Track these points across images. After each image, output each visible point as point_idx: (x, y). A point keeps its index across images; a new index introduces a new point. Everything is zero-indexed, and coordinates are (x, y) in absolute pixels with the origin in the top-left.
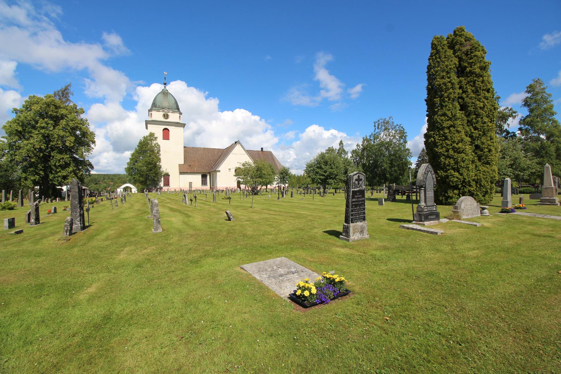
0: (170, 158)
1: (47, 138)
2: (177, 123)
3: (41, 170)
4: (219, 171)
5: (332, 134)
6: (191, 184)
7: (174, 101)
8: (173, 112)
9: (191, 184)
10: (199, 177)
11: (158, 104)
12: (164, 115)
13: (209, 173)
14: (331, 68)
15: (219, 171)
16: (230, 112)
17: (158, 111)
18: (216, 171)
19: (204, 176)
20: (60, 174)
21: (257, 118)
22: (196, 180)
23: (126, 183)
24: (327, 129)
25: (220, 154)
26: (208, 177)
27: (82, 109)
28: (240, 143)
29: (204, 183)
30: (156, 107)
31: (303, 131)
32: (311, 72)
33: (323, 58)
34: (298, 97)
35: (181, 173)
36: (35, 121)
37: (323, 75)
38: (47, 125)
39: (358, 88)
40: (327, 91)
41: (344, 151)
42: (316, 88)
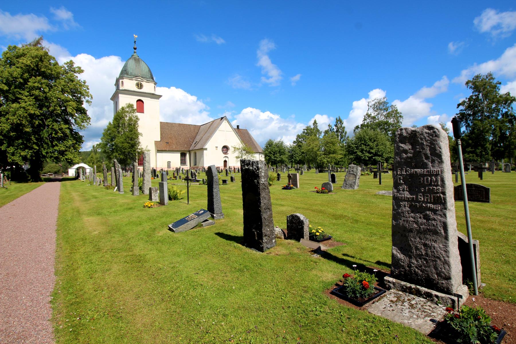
0: (148, 136)
1: (42, 102)
2: (153, 94)
3: (34, 143)
4: (206, 149)
5: (268, 116)
6: (169, 163)
7: (147, 70)
8: (148, 81)
9: (169, 163)
10: (178, 155)
11: (130, 70)
12: (137, 85)
13: (189, 151)
14: (273, 56)
15: (206, 149)
16: (167, 89)
17: (131, 79)
18: (202, 149)
19: (183, 155)
20: (56, 148)
21: (194, 98)
22: (175, 159)
23: (85, 163)
24: (263, 111)
25: (196, 131)
26: (188, 156)
27: (80, 68)
28: (226, 119)
29: (183, 162)
30: (127, 74)
31: (239, 112)
32: (255, 59)
33: (266, 45)
34: (237, 81)
35: (159, 151)
36: (23, 79)
37: (265, 61)
38: (41, 84)
39: (297, 77)
40: (268, 78)
41: (318, 131)
42: (258, 73)
